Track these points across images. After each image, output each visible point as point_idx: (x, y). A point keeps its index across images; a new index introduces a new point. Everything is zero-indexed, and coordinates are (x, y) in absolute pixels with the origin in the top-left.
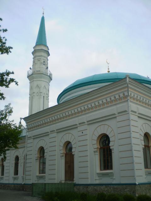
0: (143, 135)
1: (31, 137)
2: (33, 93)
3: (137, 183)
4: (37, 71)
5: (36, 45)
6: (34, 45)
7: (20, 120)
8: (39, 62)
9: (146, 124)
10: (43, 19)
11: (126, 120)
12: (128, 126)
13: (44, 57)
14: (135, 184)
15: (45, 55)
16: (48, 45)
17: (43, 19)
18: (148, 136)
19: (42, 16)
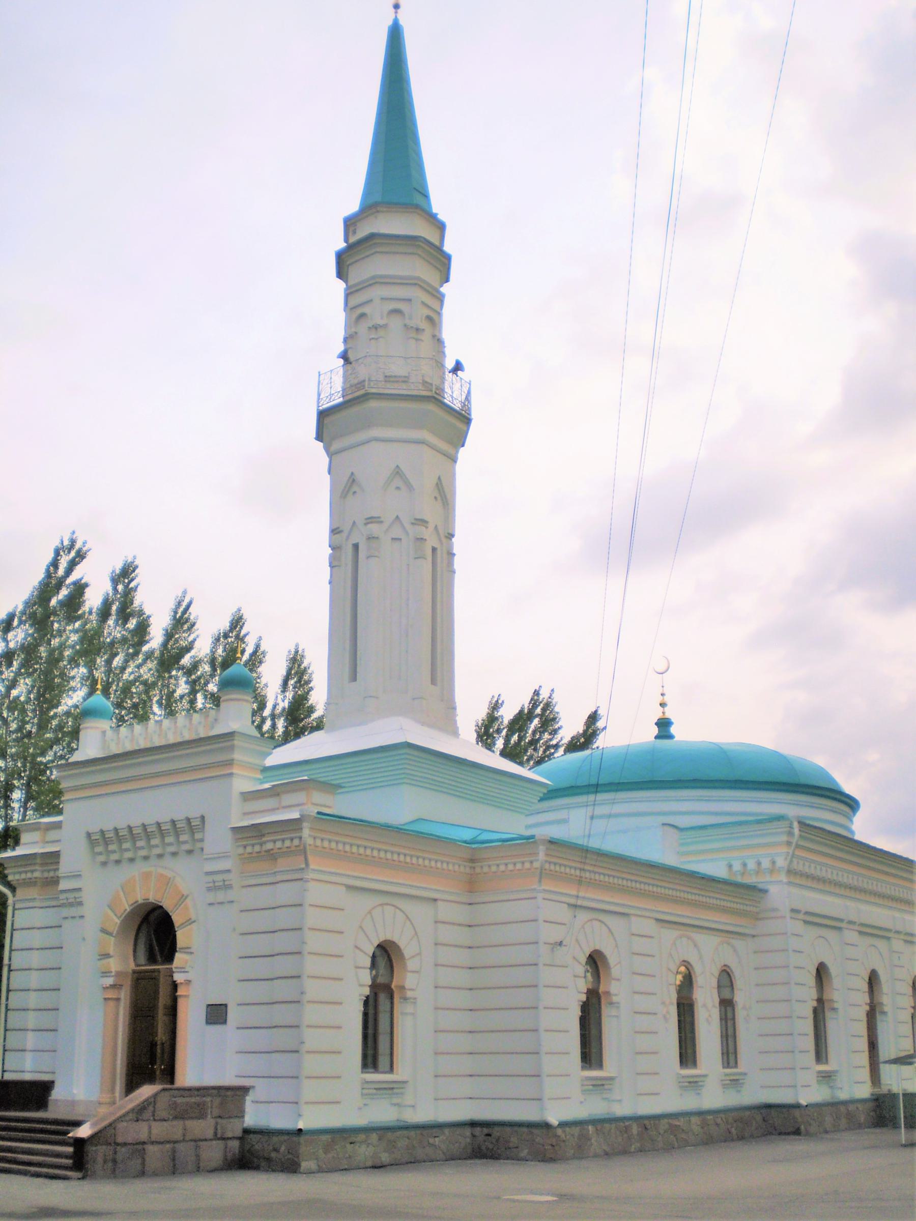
0: (583, 959)
1: (855, 923)
2: (370, 520)
3: (554, 1121)
4: (388, 379)
5: (369, 208)
6: (353, 206)
7: (394, 10)
8: (396, 323)
9: (595, 922)
10: (395, 36)
11: (22, 950)
12: (57, 929)
13: (416, 283)
14: (547, 1126)
15: (424, 272)
16: (439, 205)
17: (395, 36)
18: (599, 964)
19: (390, 23)
